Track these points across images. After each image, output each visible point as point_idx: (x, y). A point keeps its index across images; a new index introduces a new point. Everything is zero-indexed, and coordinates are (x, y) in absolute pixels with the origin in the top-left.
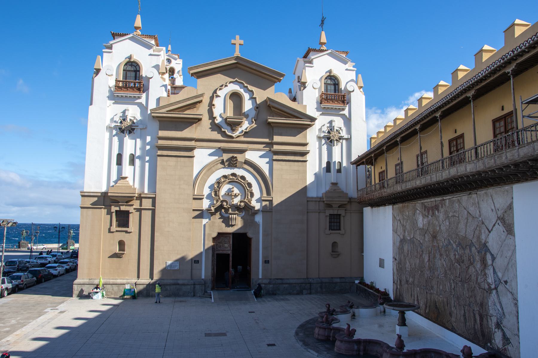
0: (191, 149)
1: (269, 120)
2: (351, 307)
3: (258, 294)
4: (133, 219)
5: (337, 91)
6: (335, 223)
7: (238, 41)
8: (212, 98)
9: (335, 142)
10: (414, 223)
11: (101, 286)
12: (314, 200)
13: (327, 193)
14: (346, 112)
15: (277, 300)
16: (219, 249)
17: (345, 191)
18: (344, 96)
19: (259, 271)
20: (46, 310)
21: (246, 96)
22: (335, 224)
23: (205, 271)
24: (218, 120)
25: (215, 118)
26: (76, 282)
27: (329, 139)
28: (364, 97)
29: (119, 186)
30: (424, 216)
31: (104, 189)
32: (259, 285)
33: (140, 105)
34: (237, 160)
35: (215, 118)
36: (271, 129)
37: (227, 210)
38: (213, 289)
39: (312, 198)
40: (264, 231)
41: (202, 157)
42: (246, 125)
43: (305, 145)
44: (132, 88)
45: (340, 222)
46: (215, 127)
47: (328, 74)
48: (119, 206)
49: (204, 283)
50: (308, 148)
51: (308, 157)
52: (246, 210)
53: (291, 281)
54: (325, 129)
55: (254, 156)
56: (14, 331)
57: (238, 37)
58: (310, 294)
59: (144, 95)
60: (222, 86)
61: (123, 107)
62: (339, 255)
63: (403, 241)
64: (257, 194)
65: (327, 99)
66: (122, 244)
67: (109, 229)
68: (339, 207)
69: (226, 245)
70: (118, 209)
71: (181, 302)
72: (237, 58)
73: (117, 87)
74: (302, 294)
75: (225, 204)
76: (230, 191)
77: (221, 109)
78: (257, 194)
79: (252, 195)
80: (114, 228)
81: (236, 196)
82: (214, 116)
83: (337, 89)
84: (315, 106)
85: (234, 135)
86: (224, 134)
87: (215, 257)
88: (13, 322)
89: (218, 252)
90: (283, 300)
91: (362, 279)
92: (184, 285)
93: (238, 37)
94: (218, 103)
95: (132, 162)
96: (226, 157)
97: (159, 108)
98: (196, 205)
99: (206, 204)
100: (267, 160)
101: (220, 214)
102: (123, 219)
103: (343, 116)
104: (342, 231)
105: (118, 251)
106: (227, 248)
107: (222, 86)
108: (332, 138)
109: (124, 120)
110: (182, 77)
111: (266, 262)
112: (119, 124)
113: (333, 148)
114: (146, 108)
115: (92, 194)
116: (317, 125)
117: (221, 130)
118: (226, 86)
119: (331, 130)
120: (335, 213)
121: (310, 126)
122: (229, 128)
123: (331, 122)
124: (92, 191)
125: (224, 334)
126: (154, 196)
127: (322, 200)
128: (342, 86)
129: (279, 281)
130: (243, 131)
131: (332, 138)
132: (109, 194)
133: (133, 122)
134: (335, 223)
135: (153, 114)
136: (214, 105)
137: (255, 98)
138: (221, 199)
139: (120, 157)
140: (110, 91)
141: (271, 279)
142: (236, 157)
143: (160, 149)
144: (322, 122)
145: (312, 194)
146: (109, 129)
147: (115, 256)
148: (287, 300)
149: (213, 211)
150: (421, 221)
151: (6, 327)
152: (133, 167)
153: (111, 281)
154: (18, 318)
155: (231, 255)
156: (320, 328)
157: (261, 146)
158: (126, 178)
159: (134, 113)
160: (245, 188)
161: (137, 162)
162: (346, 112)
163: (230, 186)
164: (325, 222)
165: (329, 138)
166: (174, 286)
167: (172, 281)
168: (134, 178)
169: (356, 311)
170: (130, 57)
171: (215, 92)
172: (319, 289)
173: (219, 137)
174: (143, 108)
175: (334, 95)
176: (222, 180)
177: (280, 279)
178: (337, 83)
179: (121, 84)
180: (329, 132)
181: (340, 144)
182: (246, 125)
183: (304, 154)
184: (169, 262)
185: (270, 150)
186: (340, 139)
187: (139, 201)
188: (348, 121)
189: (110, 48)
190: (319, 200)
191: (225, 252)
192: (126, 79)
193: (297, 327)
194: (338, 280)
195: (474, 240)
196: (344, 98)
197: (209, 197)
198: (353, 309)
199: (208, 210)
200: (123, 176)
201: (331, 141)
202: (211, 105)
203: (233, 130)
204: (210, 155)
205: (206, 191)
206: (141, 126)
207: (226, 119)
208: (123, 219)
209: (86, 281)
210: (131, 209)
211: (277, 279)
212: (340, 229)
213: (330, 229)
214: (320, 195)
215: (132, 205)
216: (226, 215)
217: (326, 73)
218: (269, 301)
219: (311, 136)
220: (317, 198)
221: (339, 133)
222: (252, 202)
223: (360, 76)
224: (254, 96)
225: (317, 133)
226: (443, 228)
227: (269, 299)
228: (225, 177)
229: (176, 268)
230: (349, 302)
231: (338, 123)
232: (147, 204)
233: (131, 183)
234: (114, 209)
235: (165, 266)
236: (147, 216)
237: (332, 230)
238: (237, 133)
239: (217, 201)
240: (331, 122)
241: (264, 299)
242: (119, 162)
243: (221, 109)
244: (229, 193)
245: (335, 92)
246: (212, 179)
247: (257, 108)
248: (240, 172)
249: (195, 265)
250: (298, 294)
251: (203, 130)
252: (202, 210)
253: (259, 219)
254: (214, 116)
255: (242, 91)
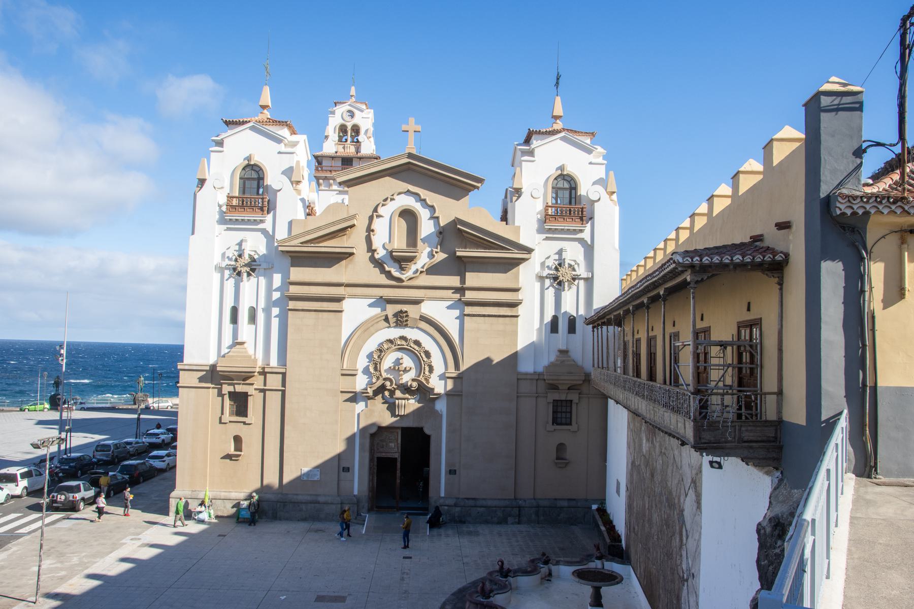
0: (339, 300)
1: (458, 254)
2: (546, 562)
3: (435, 523)
4: (254, 405)
5: (573, 200)
6: (562, 414)
7: (412, 125)
8: (371, 219)
9: (566, 284)
10: (640, 445)
11: (207, 502)
12: (529, 377)
13: (552, 365)
14: (586, 235)
15: (460, 534)
16: (381, 450)
17: (580, 363)
18: (582, 208)
19: (441, 486)
20: (124, 541)
21: (424, 215)
22: (564, 415)
23: (358, 483)
24: (380, 253)
25: (375, 250)
26: (173, 494)
27: (557, 280)
28: (617, 208)
29: (232, 356)
30: (648, 440)
31: (211, 361)
32: (437, 508)
33: (264, 232)
34: (407, 316)
35: (375, 250)
36: (459, 266)
37: (392, 392)
38: (370, 510)
39: (526, 374)
40: (449, 424)
41: (357, 311)
42: (423, 260)
43: (516, 290)
44: (251, 207)
45: (571, 412)
46: (378, 264)
47: (559, 172)
48: (233, 385)
49: (358, 501)
50: (520, 296)
51: (520, 310)
52: (422, 391)
53: (489, 503)
54: (551, 263)
55: (439, 310)
56: (70, 578)
57: (412, 120)
58: (519, 523)
59: (269, 218)
60: (386, 200)
61: (238, 236)
62: (567, 464)
63: (633, 463)
64: (439, 368)
65: (555, 217)
66: (238, 440)
67: (220, 418)
68: (569, 389)
69: (392, 445)
70: (231, 389)
71: (317, 531)
72: (410, 156)
73: (231, 207)
74: (506, 523)
75: (388, 383)
76: (398, 362)
77: (387, 235)
78: (439, 368)
79: (431, 369)
80: (227, 417)
81: (406, 371)
82: (373, 248)
83: (573, 196)
84: (535, 226)
85: (403, 277)
86: (389, 275)
87: (375, 463)
88: (75, 560)
89: (379, 455)
90: (470, 533)
91: (602, 502)
92: (326, 503)
93: (412, 120)
94: (381, 227)
95: (253, 319)
96: (391, 309)
97: (291, 237)
98: (345, 384)
99: (361, 383)
100: (457, 313)
101: (383, 398)
102: (240, 403)
103: (582, 241)
104: (574, 427)
105: (232, 451)
106: (393, 449)
107: (386, 200)
108: (561, 278)
109: (240, 256)
110: (372, 139)
111: (452, 472)
112: (233, 263)
113: (563, 293)
114: (273, 237)
115: (195, 368)
116: (536, 259)
117: (384, 268)
118: (392, 199)
119: (560, 265)
120: (563, 398)
121: (524, 260)
122: (397, 265)
123: (560, 253)
124: (195, 362)
125: (342, 599)
126: (283, 370)
127: (541, 377)
128: (582, 191)
129: (471, 503)
130: (417, 270)
131: (561, 278)
132: (218, 369)
133: (254, 260)
134: (562, 414)
135: (281, 249)
136: (373, 231)
137: (437, 218)
138: (384, 375)
139: (235, 311)
140: (222, 213)
141: (458, 498)
142: (406, 312)
143: (288, 302)
144: (543, 251)
145: (526, 367)
146: (221, 270)
147: (228, 457)
148: (477, 534)
149: (371, 394)
150: (645, 446)
151: (62, 569)
152: (253, 327)
153: (223, 495)
154: (84, 554)
155: (399, 460)
156: (471, 602)
157: (449, 293)
158: (242, 343)
159: (256, 245)
160: (421, 358)
161: (261, 317)
162: (586, 235)
163: (399, 354)
164: (546, 412)
165: (555, 278)
166: (313, 505)
167: (309, 498)
168: (255, 346)
169: (554, 568)
170: (249, 158)
171: (375, 210)
172: (533, 516)
173: (383, 280)
174: (270, 237)
175: (569, 206)
176: (386, 346)
177: (473, 499)
178: (573, 186)
179: (235, 202)
180: (556, 269)
181: (574, 288)
182: (423, 260)
183: (514, 305)
184: (305, 470)
185: (460, 300)
186: (574, 279)
187: (263, 377)
188: (589, 250)
189: (220, 144)
190: (537, 377)
191: (389, 455)
192: (244, 193)
193: (455, 590)
194: (565, 504)
195: (676, 501)
196: (582, 212)
197: (366, 371)
198: (550, 565)
199: (365, 391)
200: (239, 340)
201: (560, 283)
202: (370, 230)
203: (402, 269)
204: (370, 306)
205: (362, 362)
206: (264, 265)
207: (391, 252)
208: (240, 403)
209: (188, 493)
210: (250, 390)
211: (468, 499)
212: (570, 424)
213: (555, 421)
214: (540, 369)
215: (252, 384)
216: (391, 401)
217: (557, 169)
218: (447, 536)
219: (527, 277)
220: (535, 373)
221: (574, 270)
222: (430, 380)
223: (612, 173)
224: (436, 215)
225: (538, 269)
226: (658, 467)
227: (450, 532)
228: (390, 341)
229: (316, 479)
230: (544, 554)
231: (574, 253)
232: (274, 381)
233: (251, 351)
234: (226, 389)
235: (299, 474)
236: (274, 399)
237: (558, 424)
238: (409, 273)
239: (378, 378)
240: (560, 253)
241: (442, 531)
242: (234, 319)
243: (387, 235)
244: (397, 367)
245: (570, 203)
246: (371, 345)
247: (441, 233)
248: (412, 334)
249: (343, 474)
250: (499, 523)
251: (359, 269)
252: (355, 392)
253: (441, 406)
254: (373, 248)
255: (417, 207)
